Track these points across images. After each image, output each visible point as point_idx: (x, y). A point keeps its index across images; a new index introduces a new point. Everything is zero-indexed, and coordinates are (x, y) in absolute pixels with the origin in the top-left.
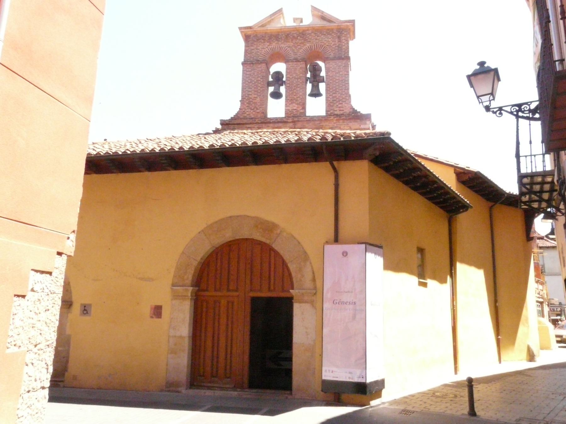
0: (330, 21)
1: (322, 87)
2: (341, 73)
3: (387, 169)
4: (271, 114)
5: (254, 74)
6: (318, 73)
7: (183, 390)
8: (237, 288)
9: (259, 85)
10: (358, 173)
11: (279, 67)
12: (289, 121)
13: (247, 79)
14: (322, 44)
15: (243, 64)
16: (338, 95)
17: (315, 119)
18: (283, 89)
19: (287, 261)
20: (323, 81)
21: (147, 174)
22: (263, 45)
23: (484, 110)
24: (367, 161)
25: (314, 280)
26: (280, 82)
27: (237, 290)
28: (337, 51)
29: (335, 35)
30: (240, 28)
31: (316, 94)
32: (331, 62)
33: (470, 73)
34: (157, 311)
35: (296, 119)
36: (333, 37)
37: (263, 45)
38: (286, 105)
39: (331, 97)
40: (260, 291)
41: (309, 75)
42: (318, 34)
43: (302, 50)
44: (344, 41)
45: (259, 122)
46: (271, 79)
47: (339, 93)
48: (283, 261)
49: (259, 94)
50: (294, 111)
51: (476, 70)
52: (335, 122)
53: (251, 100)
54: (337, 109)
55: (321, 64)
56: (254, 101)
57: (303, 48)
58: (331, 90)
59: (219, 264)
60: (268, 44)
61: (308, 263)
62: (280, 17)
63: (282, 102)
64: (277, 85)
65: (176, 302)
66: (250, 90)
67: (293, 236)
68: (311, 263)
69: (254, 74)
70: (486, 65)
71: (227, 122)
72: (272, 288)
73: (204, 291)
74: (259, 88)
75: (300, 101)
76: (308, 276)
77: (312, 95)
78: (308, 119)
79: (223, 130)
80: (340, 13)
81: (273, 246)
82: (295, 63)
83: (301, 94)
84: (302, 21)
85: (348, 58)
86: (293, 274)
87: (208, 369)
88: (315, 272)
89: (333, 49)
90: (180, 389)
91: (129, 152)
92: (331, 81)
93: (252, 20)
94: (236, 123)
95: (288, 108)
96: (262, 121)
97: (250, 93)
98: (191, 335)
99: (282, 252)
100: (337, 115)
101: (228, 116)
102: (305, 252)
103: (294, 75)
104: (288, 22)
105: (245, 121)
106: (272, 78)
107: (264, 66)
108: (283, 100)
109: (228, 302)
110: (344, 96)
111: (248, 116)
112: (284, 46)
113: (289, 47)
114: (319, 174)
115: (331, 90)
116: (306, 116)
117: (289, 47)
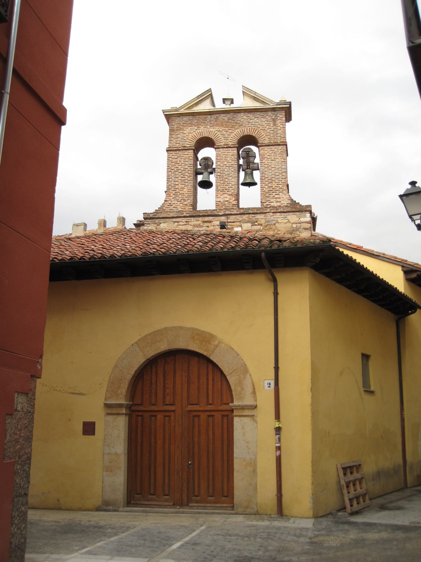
0: (263, 102)
1: (256, 174)
6: (251, 159)
8: (173, 403)
14: (256, 128)
16: (274, 185)
18: (212, 178)
20: (258, 169)
23: (416, 228)
25: (254, 393)
26: (209, 170)
29: (269, 119)
30: (164, 111)
33: (402, 194)
35: (227, 212)
39: (266, 187)
44: (279, 124)
45: (188, 215)
46: (199, 167)
50: (226, 203)
51: (408, 190)
53: (178, 191)
58: (266, 180)
59: (154, 377)
60: (196, 128)
61: (248, 376)
66: (176, 179)
68: (250, 375)
70: (417, 185)
72: (210, 402)
77: (244, 184)
78: (242, 211)
81: (211, 358)
84: (232, 102)
86: (233, 387)
89: (268, 134)
92: (266, 169)
93: (178, 101)
94: (161, 216)
95: (219, 200)
96: (191, 214)
97: (177, 183)
98: (126, 452)
103: (226, 163)
105: (171, 215)
106: (200, 165)
108: (212, 190)
110: (281, 186)
113: (219, 131)
115: (266, 180)
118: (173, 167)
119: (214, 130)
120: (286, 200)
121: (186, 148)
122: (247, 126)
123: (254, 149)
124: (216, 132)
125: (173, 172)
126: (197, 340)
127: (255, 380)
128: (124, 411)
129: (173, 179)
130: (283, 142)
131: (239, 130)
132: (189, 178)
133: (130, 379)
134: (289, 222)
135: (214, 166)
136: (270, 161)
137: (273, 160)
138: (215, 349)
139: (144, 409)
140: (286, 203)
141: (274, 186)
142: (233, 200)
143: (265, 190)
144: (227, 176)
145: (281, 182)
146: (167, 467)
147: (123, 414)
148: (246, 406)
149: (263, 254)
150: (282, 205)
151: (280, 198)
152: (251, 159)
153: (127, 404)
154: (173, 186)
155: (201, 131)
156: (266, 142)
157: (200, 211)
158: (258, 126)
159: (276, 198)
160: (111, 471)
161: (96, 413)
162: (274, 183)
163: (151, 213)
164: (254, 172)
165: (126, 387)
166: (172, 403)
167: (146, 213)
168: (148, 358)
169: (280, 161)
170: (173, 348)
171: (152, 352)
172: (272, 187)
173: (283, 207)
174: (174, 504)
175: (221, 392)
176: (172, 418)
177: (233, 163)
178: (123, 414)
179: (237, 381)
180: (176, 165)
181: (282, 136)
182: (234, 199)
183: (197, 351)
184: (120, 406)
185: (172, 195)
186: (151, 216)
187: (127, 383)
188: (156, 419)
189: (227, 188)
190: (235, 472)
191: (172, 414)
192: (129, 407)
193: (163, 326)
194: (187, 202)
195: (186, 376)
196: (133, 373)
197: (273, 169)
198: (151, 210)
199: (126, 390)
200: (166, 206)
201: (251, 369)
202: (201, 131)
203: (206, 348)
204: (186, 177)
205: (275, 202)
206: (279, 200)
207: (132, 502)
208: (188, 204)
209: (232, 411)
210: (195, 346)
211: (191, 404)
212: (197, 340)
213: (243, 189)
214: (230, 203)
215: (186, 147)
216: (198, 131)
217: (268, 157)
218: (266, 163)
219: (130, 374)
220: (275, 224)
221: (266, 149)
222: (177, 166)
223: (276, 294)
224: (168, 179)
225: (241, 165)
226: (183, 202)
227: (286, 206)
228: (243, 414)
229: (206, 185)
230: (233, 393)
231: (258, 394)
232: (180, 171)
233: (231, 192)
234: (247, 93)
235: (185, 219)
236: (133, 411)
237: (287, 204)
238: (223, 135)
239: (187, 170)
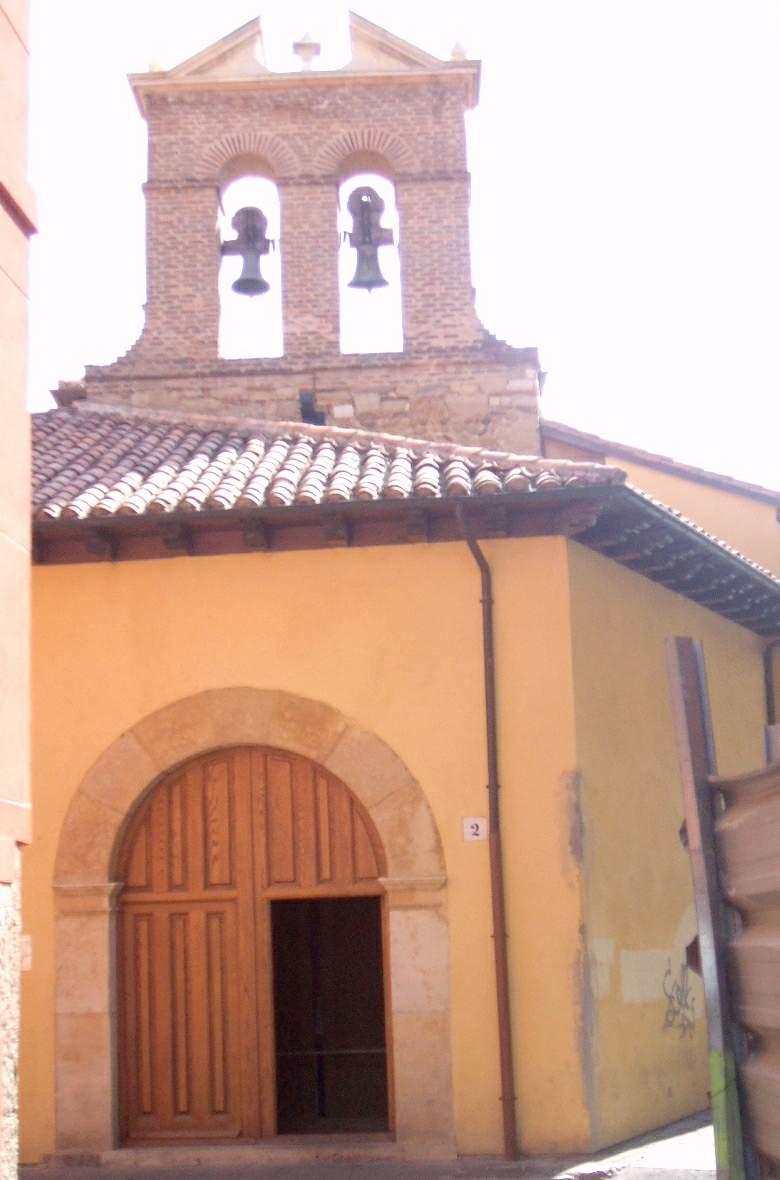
1: (389, 258)
2: (445, 223)
5: (180, 220)
7: (109, 1155)
8: (231, 880)
9: (200, 257)
10: (541, 575)
12: (294, 368)
13: (161, 239)
15: (150, 188)
17: (375, 362)
22: (202, 125)
25: (438, 849)
27: (231, 884)
28: (431, 152)
30: (132, 78)
31: (369, 277)
35: (316, 364)
37: (202, 125)
40: (295, 881)
42: (374, 98)
43: (325, 147)
44: (450, 122)
45: (207, 371)
47: (439, 281)
48: (353, 800)
49: (200, 285)
50: (310, 338)
52: (433, 370)
54: (438, 332)
56: (187, 307)
57: (330, 142)
58: (418, 275)
59: (177, 814)
60: (220, 127)
61: (422, 808)
63: (271, 302)
65: (70, 924)
66: (171, 271)
67: (380, 741)
68: (428, 807)
69: (180, 220)
71: (107, 372)
72: (326, 874)
73: (140, 889)
74: (199, 266)
75: (327, 306)
76: (424, 841)
77: (357, 283)
80: (436, 42)
81: (328, 765)
82: (306, 189)
85: (464, 177)
86: (385, 837)
87: (201, 1084)
88: (441, 830)
92: (417, 247)
93: (172, 50)
95: (291, 329)
97: (173, 282)
99: (351, 781)
100: (440, 351)
102: (413, 782)
103: (306, 227)
104: (275, 59)
105: (162, 369)
109: (209, 915)
110: (457, 293)
111: (170, 354)
113: (285, 137)
114: (439, 572)
117: (285, 137)
127: (440, 817)
134: (480, 389)
147: (103, 912)
155: (234, 136)
159: (445, 326)
166: (227, 880)
167: (91, 366)
168: (164, 768)
171: (173, 756)
173: (464, 349)
174: (240, 1134)
175: (252, 825)
176: (230, 917)
185: (160, 313)
191: (228, 908)
193: (202, 686)
195: (261, 812)
198: (106, 358)
201: (429, 789)
202: (234, 136)
216: (228, 136)
219: (115, 809)
220: (441, 397)
222: (171, 232)
227: (473, 349)
231: (448, 852)
234: (368, 34)
235: (199, 383)
237: (475, 341)
238: (298, 150)
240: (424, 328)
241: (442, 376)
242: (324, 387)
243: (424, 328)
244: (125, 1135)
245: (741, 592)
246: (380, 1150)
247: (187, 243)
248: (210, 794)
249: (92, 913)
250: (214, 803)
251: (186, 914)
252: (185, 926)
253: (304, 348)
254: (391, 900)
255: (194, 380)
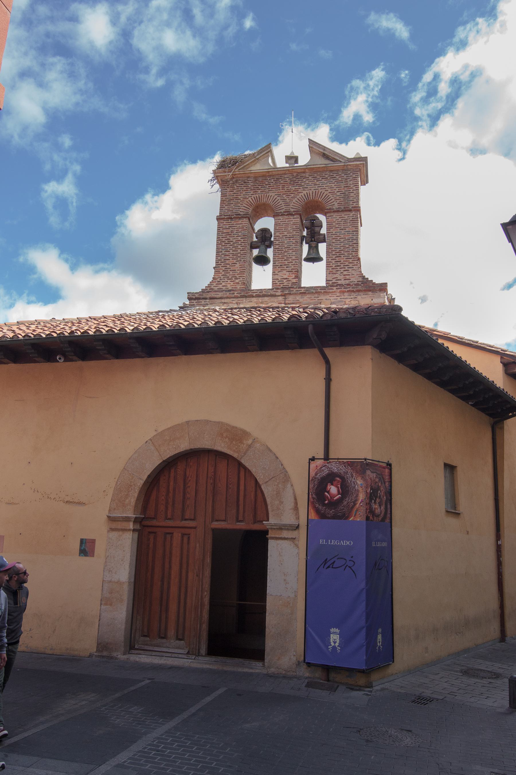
0: (333, 160)
1: (322, 248)
2: (347, 230)
3: (400, 359)
4: (306, 282)
5: (232, 232)
6: (317, 229)
11: (266, 223)
12: (277, 294)
14: (323, 191)
18: (270, 253)
19: (261, 483)
20: (324, 241)
21: (80, 363)
24: (370, 347)
26: (267, 243)
31: (314, 258)
32: (335, 215)
34: (86, 548)
36: (338, 182)
38: (274, 274)
41: (305, 233)
45: (239, 295)
46: (255, 239)
50: (285, 281)
53: (228, 266)
55: (322, 218)
59: (172, 483)
61: (289, 486)
62: (268, 156)
63: (321, 267)
64: (263, 247)
65: (114, 535)
66: (227, 253)
68: (292, 485)
69: (232, 232)
72: (241, 518)
77: (307, 260)
78: (303, 290)
79: (192, 306)
81: (243, 461)
83: (294, 258)
84: (296, 161)
85: (358, 210)
86: (268, 500)
88: (297, 498)
89: (338, 198)
90: (115, 654)
91: (55, 335)
92: (334, 241)
95: (276, 277)
97: (227, 257)
98: (133, 580)
101: (198, 287)
103: (286, 233)
105: (220, 295)
106: (257, 238)
107: (246, 221)
108: (269, 267)
109: (183, 535)
112: (272, 196)
113: (279, 195)
116: (300, 287)
118: (224, 239)
119: (273, 194)
120: (357, 277)
121: (240, 216)
122: (312, 189)
123: (322, 218)
124: (276, 196)
125: (223, 245)
126: (226, 437)
128: (131, 526)
129: (223, 253)
130: (355, 207)
131: (302, 194)
132: (242, 252)
133: (141, 486)
135: (272, 239)
136: (339, 231)
137: (343, 229)
138: (247, 450)
139: (158, 524)
140: (356, 281)
141: (342, 261)
142: (294, 277)
143: (331, 265)
144: (287, 249)
145: (351, 255)
146: (182, 601)
147: (130, 530)
148: (285, 525)
149: (310, 328)
150: (351, 283)
151: (349, 275)
152: (317, 229)
153: (136, 518)
154: (223, 261)
156: (336, 206)
157: (253, 290)
158: (328, 190)
160: (111, 605)
161: (96, 527)
162: (342, 257)
163: (196, 293)
164: (319, 244)
165: (136, 495)
169: (351, 230)
170: (196, 447)
171: (169, 452)
172: (340, 261)
174: (188, 653)
177: (294, 233)
178: (130, 530)
179: (275, 493)
180: (228, 236)
181: (355, 199)
182: (294, 276)
183: (225, 452)
184: (127, 519)
185: (221, 271)
186: (197, 296)
187: (137, 491)
188: (172, 537)
189: (287, 263)
190: (267, 614)
192: (136, 520)
193: (185, 419)
194: (239, 280)
196: (145, 477)
197: (342, 240)
199: (135, 499)
200: (215, 284)
203: (236, 448)
204: (239, 250)
205: (343, 279)
206: (348, 277)
207: (136, 647)
208: (240, 282)
209: (266, 532)
210: (223, 445)
211: (217, 521)
212: (226, 437)
213: (305, 265)
214: (290, 281)
215: (239, 215)
216: (255, 196)
217: (337, 226)
218: (334, 233)
219: (141, 479)
221: (334, 217)
223: (328, 380)
224: (217, 252)
225: (304, 236)
226: (234, 280)
227: (357, 285)
228: (280, 536)
229: (262, 260)
230: (269, 507)
232: (232, 243)
233: (291, 268)
236: (145, 526)
239: (240, 242)
240: (335, 276)
241: (342, 297)
242: (289, 302)
243: (335, 276)
244: (131, 647)
245: (477, 390)
246: (255, 667)
247: (234, 240)
248: (188, 473)
249: (124, 530)
250: (190, 478)
251: (173, 533)
252: (171, 539)
253: (282, 285)
254: (270, 535)
255: (234, 299)
